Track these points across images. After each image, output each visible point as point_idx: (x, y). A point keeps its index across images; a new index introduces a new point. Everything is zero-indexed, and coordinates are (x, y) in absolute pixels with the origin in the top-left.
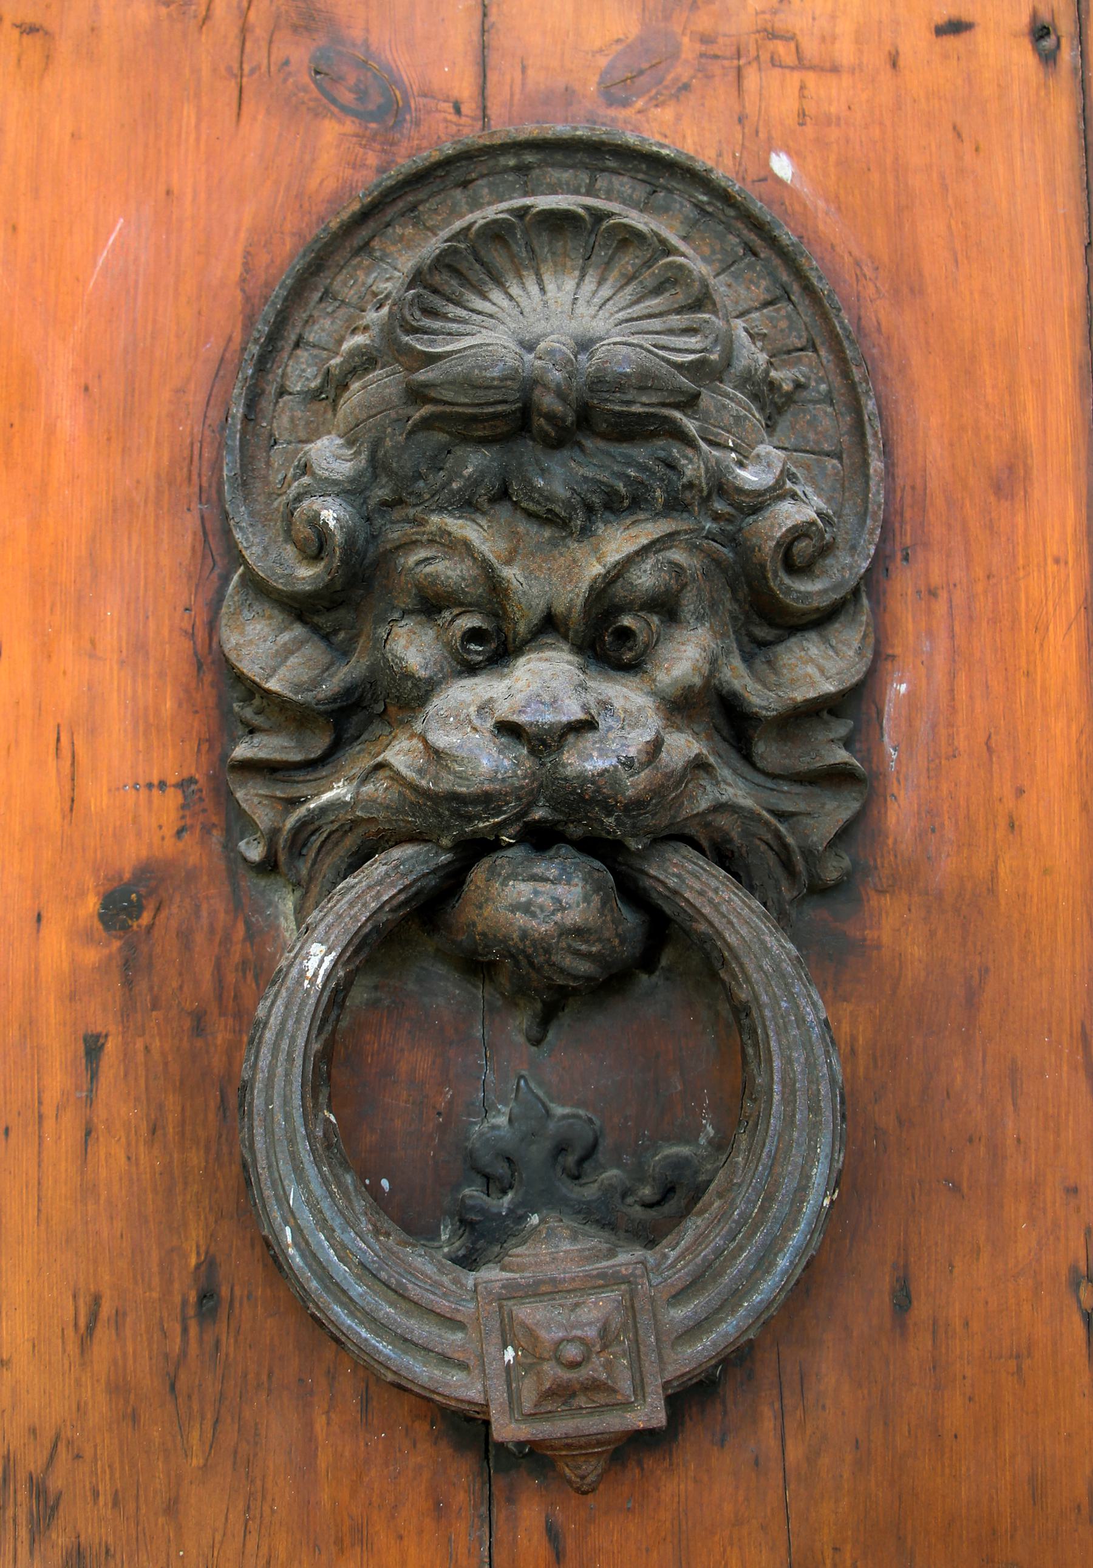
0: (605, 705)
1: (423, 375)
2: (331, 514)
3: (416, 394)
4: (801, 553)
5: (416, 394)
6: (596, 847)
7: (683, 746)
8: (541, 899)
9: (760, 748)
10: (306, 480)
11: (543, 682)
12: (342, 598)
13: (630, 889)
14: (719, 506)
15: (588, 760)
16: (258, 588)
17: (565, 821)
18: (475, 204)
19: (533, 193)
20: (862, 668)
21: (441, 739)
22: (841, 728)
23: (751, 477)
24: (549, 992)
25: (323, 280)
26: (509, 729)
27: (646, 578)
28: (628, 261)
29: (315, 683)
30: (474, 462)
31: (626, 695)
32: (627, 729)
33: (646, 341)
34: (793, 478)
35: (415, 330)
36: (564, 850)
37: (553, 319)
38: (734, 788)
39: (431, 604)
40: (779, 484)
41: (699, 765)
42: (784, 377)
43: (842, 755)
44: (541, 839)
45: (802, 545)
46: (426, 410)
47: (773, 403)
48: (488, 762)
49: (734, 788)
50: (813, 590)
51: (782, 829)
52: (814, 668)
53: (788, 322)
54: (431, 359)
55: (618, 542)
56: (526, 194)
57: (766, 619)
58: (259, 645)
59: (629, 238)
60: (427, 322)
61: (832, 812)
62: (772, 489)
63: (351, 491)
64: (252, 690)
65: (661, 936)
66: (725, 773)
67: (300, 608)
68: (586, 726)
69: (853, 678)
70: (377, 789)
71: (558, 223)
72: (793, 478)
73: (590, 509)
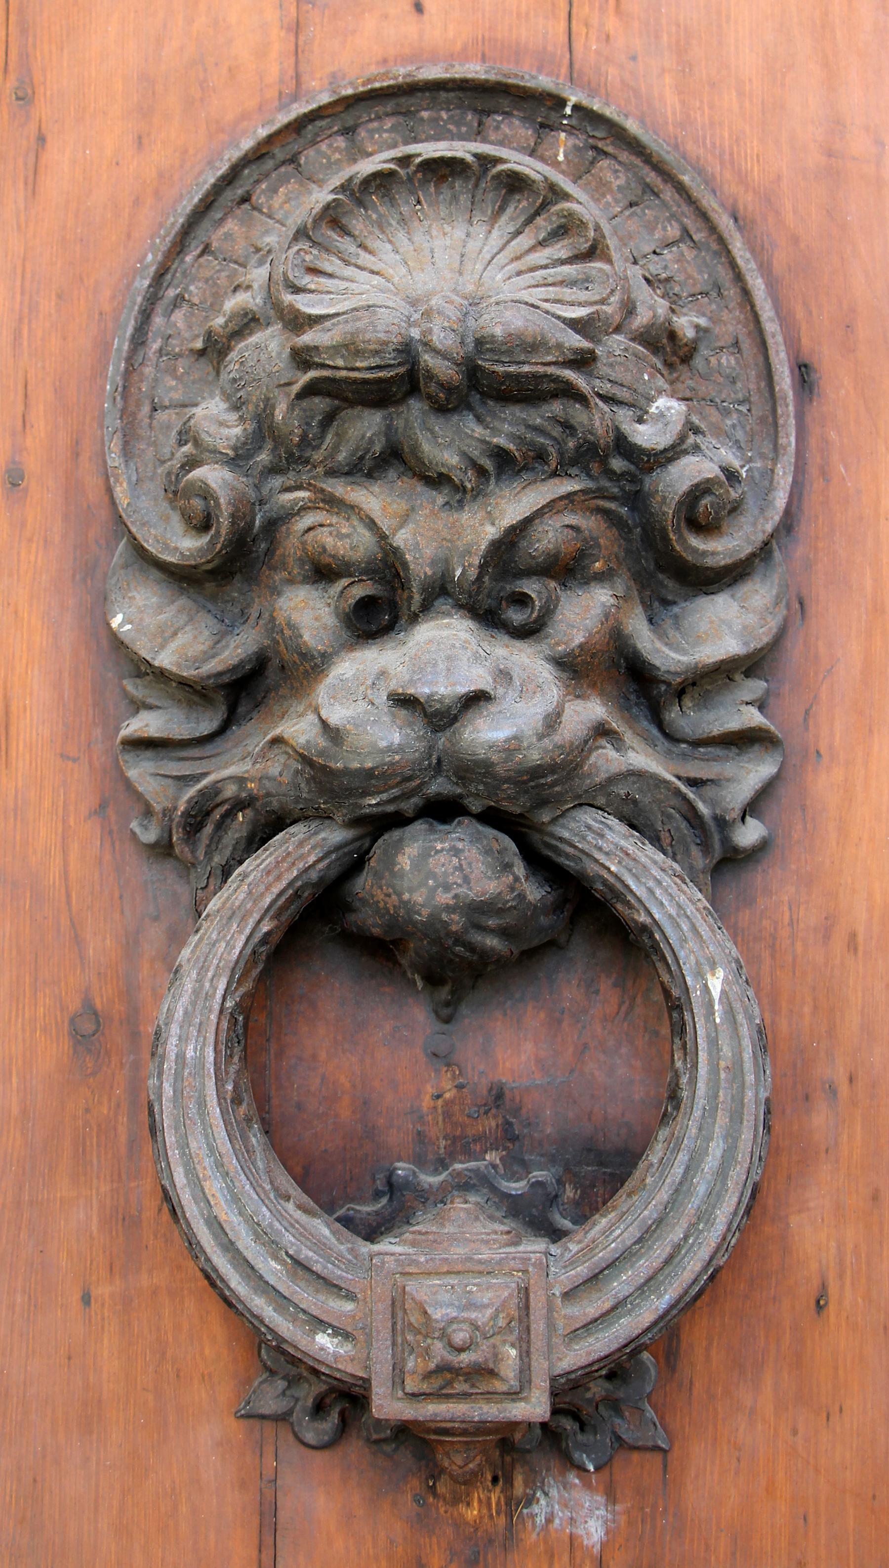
0: (504, 675)
1: (308, 338)
2: (213, 476)
3: (302, 358)
4: (702, 511)
5: (302, 358)
6: (493, 818)
7: (593, 709)
8: (445, 872)
9: (673, 714)
10: (188, 448)
11: (444, 652)
12: (232, 564)
13: (541, 861)
14: (617, 464)
15: (486, 733)
16: (143, 557)
17: (450, 791)
18: (357, 153)
19: (416, 140)
20: (774, 623)
21: (336, 715)
22: (755, 687)
23: (646, 436)
24: (452, 970)
25: (202, 233)
26: (404, 702)
27: (549, 537)
28: (520, 205)
29: (208, 656)
30: (366, 427)
31: (528, 660)
32: (521, 701)
33: (536, 295)
34: (697, 431)
35: (298, 290)
36: (466, 821)
37: (437, 277)
38: (641, 756)
39: (323, 572)
40: (682, 438)
41: (602, 731)
42: (686, 324)
43: (754, 718)
44: (443, 811)
45: (706, 501)
46: (312, 374)
47: (670, 350)
48: (387, 737)
49: (641, 756)
50: (720, 549)
51: (691, 796)
52: (720, 628)
53: (684, 265)
54: (315, 321)
55: (514, 503)
56: (406, 143)
57: (672, 575)
58: (145, 617)
59: (515, 184)
60: (307, 281)
61: (751, 773)
62: (673, 447)
63: (238, 459)
64: (144, 670)
65: (588, 918)
66: (629, 737)
67: (182, 578)
68: (476, 699)
69: (763, 637)
70: (277, 767)
71: (442, 170)
72: (697, 431)
73: (482, 472)
